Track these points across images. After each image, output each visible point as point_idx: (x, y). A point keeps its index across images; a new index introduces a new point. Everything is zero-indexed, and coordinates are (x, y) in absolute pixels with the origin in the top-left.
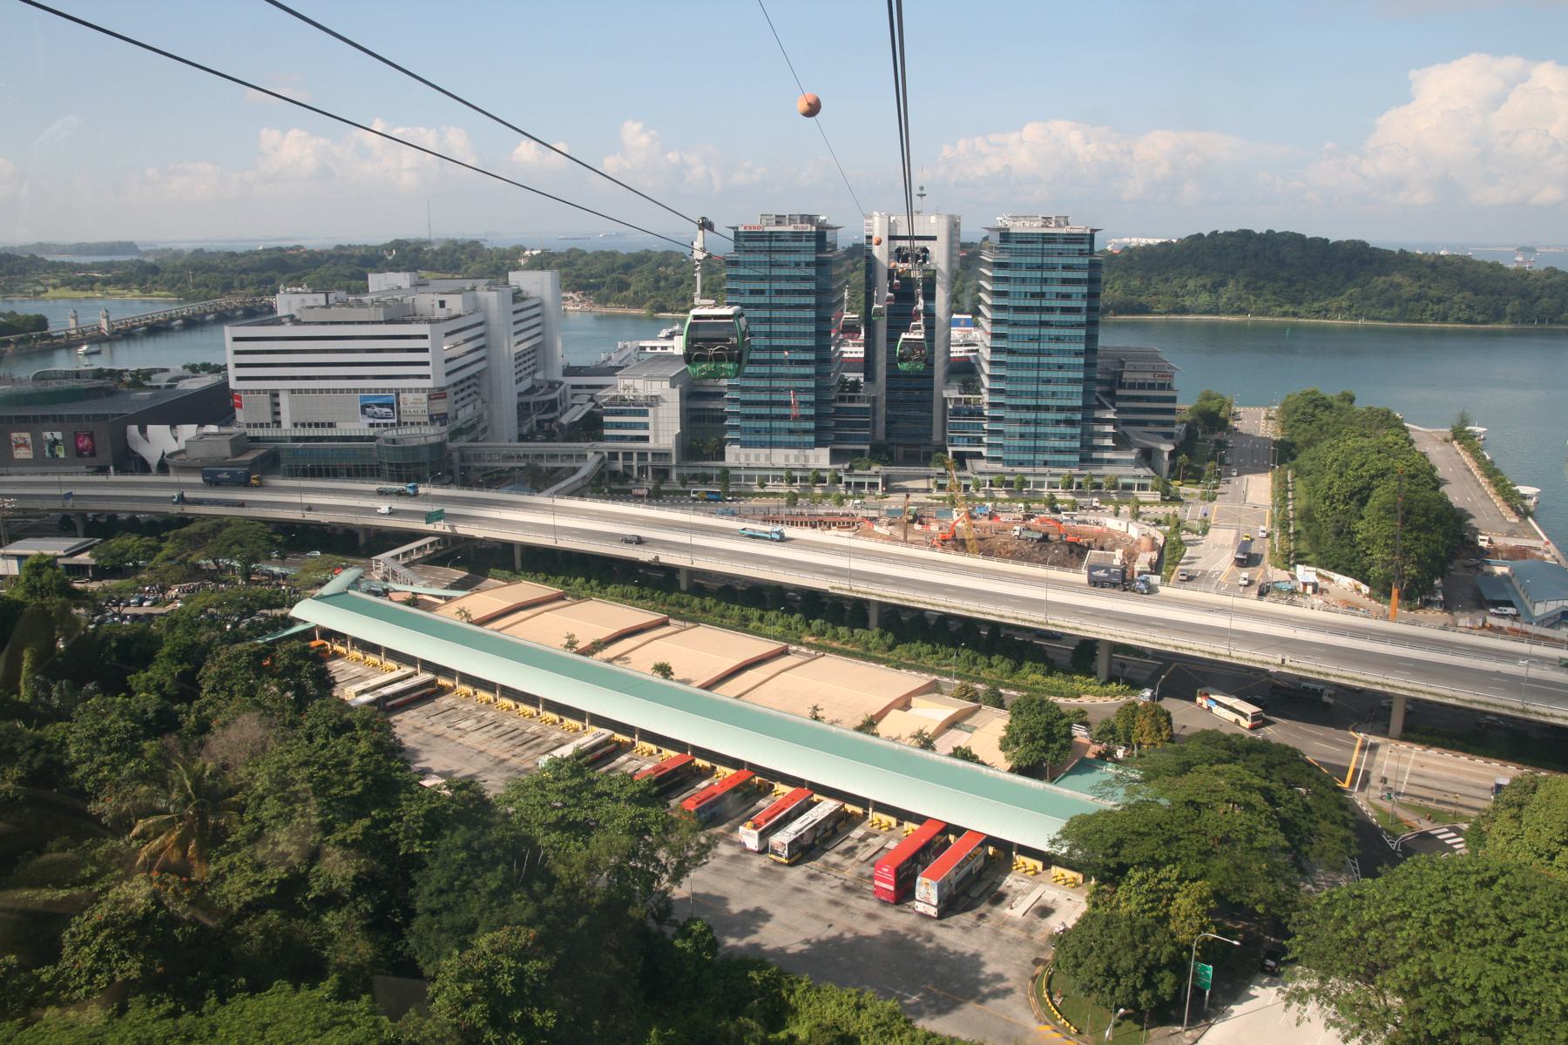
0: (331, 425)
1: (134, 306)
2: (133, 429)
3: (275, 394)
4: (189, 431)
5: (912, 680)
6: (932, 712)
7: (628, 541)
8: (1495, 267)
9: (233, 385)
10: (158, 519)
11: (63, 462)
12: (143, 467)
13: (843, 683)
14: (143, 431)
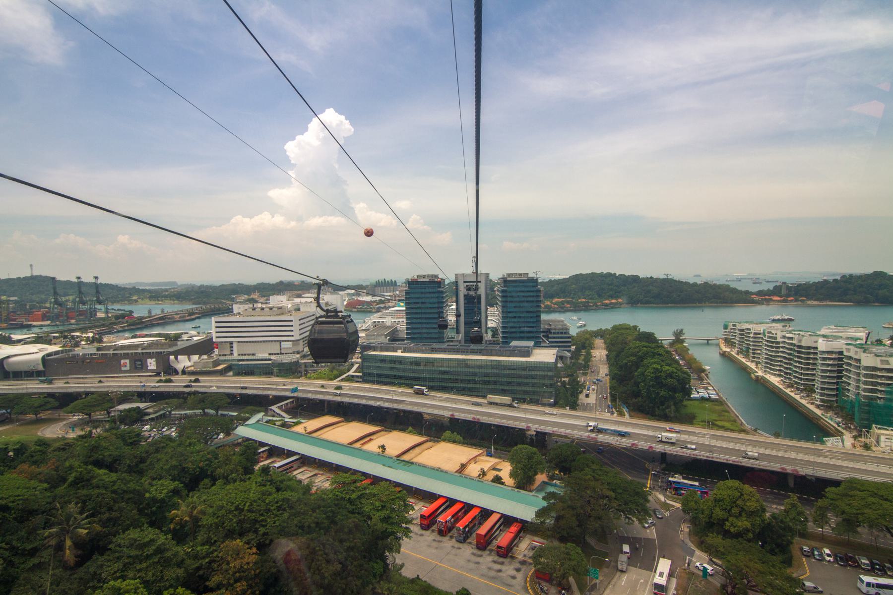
0: (254, 355)
1: (170, 308)
2: (172, 357)
3: (231, 343)
4: (195, 358)
6: (487, 463)
8: (687, 283)
9: (214, 340)
10: (839, 278)
11: (126, 356)
12: (176, 372)
14: (176, 358)
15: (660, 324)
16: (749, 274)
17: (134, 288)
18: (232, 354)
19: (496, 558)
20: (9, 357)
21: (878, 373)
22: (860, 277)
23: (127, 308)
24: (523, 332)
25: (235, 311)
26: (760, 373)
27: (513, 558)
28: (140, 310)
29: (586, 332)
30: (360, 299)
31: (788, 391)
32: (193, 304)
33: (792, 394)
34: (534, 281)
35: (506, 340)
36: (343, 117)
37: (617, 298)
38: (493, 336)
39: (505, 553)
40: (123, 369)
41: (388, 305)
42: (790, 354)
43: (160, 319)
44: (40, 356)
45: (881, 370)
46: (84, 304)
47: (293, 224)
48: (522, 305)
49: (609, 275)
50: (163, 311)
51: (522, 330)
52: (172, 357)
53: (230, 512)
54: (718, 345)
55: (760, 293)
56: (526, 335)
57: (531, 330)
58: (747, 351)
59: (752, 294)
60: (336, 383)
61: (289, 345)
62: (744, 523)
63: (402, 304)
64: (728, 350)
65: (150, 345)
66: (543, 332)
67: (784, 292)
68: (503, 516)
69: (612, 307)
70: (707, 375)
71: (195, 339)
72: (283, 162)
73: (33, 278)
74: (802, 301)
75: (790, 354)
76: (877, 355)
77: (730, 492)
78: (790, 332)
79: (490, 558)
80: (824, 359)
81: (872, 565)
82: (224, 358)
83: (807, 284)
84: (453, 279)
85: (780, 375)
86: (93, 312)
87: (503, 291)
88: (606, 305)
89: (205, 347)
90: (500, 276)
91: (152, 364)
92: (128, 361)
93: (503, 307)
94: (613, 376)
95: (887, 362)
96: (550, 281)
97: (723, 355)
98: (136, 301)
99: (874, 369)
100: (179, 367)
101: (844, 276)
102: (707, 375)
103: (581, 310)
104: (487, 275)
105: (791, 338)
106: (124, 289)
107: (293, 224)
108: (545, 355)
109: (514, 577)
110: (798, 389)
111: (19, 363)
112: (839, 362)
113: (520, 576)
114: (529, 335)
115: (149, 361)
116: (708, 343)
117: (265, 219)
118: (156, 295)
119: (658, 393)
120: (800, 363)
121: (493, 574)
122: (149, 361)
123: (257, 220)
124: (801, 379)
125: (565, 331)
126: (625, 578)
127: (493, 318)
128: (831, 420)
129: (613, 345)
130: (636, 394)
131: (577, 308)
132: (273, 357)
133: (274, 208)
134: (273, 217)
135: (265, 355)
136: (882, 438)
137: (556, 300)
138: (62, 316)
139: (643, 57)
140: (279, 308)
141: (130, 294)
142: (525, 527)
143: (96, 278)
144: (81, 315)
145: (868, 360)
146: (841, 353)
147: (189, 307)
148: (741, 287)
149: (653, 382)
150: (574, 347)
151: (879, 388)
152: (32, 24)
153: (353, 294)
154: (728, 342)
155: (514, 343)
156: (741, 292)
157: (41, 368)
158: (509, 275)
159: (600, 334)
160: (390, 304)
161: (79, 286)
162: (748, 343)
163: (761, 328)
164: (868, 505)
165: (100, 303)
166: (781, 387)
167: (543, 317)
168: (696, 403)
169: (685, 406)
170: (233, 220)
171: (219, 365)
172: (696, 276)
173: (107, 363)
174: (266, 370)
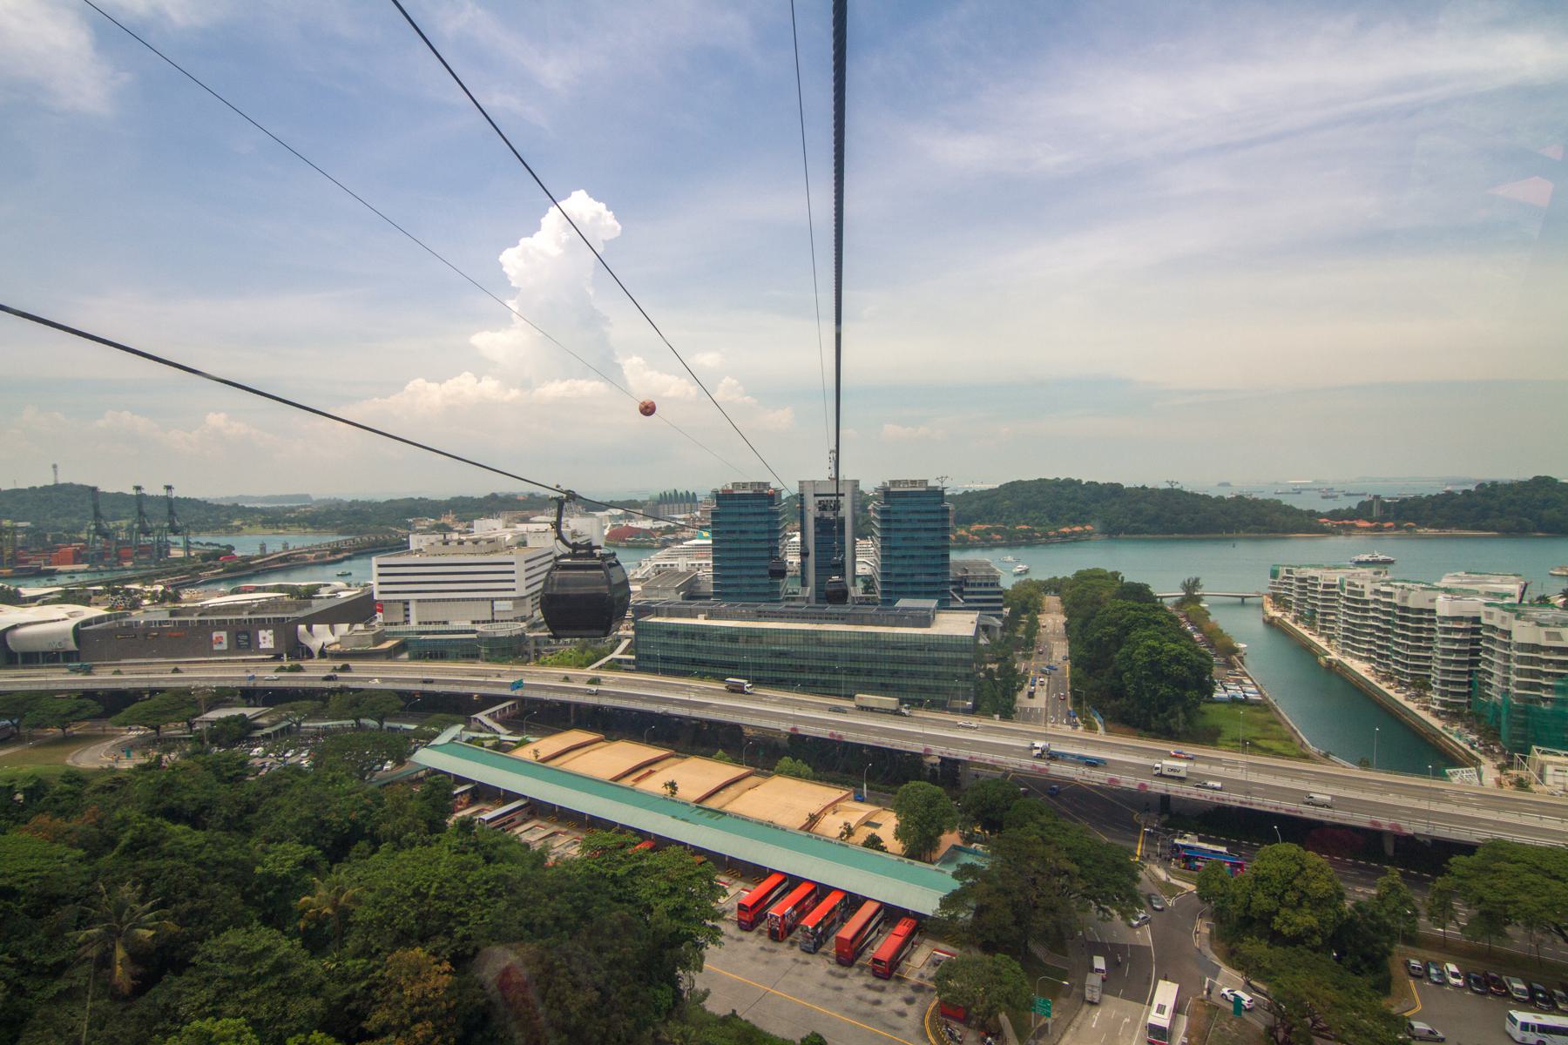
0: (445, 623)
1: (298, 540)
2: (302, 628)
3: (406, 603)
4: (343, 628)
5: (834, 793)
6: (856, 813)
7: (426, 682)
8: (1206, 498)
9: (376, 597)
10: (1472, 488)
11: (221, 625)
12: (309, 654)
13: (785, 799)
14: (310, 629)
15: (1159, 570)
16: (1316, 482)
17: (236, 505)
18: (407, 622)
19: (871, 980)
20: (15, 627)
21: (1542, 656)
22: (1511, 487)
23: (224, 540)
24: (918, 584)
25: (413, 547)
26: (1334, 656)
27: (900, 979)
28: (246, 545)
29: (1030, 583)
30: (633, 524)
31: (1383, 686)
32: (339, 534)
33: (1391, 693)
34: (938, 494)
35: (889, 598)
36: (602, 206)
37: (1083, 523)
38: (866, 590)
39: (887, 971)
40: (216, 647)
41: (681, 535)
42: (1387, 622)
43: (281, 559)
44: (70, 624)
45: (1547, 649)
46: (147, 534)
47: (514, 393)
48: (916, 535)
49: (1070, 483)
50: (286, 546)
51: (917, 579)
52: (302, 628)
53: (404, 899)
54: (1261, 606)
55: (1334, 515)
56: (924, 589)
57: (932, 579)
58: (1312, 617)
59: (1321, 516)
60: (589, 672)
61: (508, 605)
62: (1306, 919)
63: (706, 534)
64: (1279, 614)
65: (263, 607)
66: (954, 583)
67: (1376, 512)
68: (884, 906)
69: (1074, 539)
70: (1241, 659)
71: (343, 595)
72: (497, 285)
73: (58, 488)
74: (1409, 529)
75: (1387, 622)
76: (1539, 624)
77: (1281, 865)
78: (1388, 584)
79: (861, 981)
80: (1447, 631)
81: (1532, 992)
82: (394, 629)
83: (1417, 499)
84: (795, 490)
85: (1369, 659)
86: (164, 549)
87: (883, 512)
88: (1065, 536)
89: (360, 609)
90: (879, 484)
91: (266, 639)
92: (224, 634)
93: (883, 539)
94: (1076, 661)
95: (1558, 637)
96: (966, 493)
97: (1270, 623)
98: (239, 529)
99: (1535, 648)
100: (315, 645)
101: (1481, 485)
102: (1241, 659)
103: (1020, 545)
104: (856, 483)
105: (1389, 594)
106: (218, 507)
107: (514, 393)
108: (957, 624)
109: (902, 1014)
110: (1400, 683)
111: (33, 637)
112: (1473, 636)
113: (913, 1011)
114: (929, 589)
115: (262, 633)
116: (1243, 602)
117: (465, 385)
118: (273, 518)
119: (1156, 691)
120: (1404, 637)
121: (865, 1007)
122: (262, 633)
123: (451, 386)
124: (1407, 666)
125: (993, 581)
126: (1097, 1015)
127: (866, 559)
128: (1458, 737)
129: (1076, 605)
130: (1117, 693)
131: (1012, 541)
132: (479, 628)
133: (481, 366)
134: (479, 381)
135: (466, 624)
136: (1549, 769)
137: (976, 527)
138: (108, 555)
139: (1128, 99)
140: (491, 541)
141: (229, 516)
142: (921, 926)
143: (169, 488)
144: (142, 553)
145: (1524, 633)
146: (1477, 620)
147: (331, 538)
148: (1301, 504)
149: (1147, 672)
150: (1007, 610)
151: (1544, 682)
152: (56, 43)
153: (620, 517)
154: (1278, 600)
155: (903, 603)
156: (1301, 513)
157: (72, 646)
158: (894, 483)
159: (1054, 586)
160: (685, 534)
161: (139, 503)
162: (1313, 603)
163: (1336, 577)
164: (1523, 888)
165: (175, 532)
166: (1372, 679)
167: (954, 556)
168: (1223, 707)
169: (1204, 713)
170: (410, 387)
171: (385, 640)
172: (1221, 485)
173: (188, 637)
174: (468, 650)
